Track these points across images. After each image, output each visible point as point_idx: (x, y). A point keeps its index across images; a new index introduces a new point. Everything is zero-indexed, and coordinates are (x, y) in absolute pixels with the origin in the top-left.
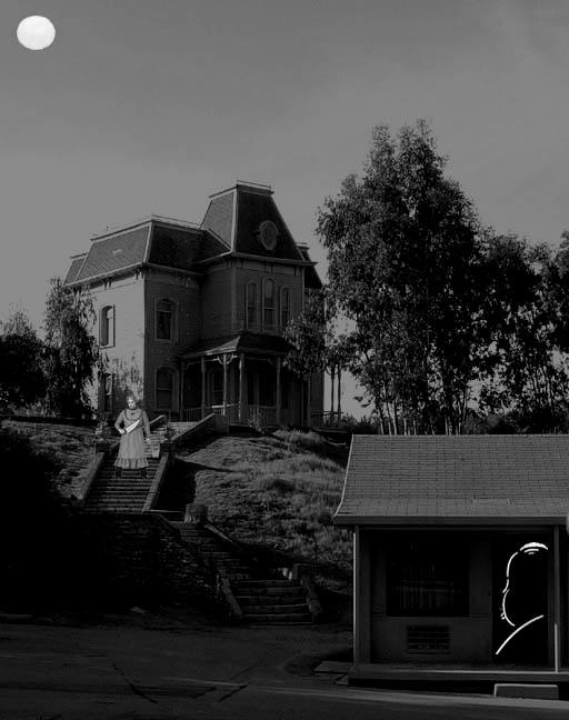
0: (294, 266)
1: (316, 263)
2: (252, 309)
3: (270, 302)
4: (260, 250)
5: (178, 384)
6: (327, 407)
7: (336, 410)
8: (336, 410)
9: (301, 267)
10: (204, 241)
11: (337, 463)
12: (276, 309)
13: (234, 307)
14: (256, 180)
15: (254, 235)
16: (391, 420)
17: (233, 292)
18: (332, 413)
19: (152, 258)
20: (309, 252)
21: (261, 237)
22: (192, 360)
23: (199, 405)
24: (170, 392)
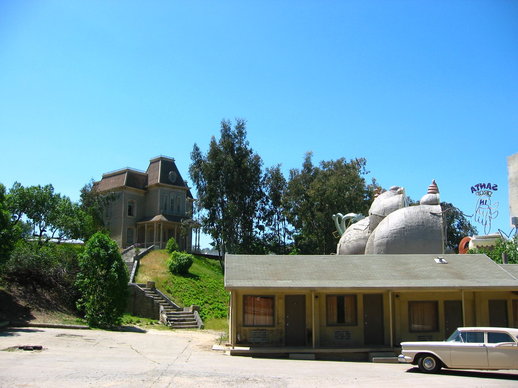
0: (183, 189)
1: (175, 160)
2: (166, 205)
3: (172, 200)
4: (169, 182)
5: (136, 233)
6: (193, 244)
7: (197, 245)
8: (197, 245)
9: (185, 190)
10: (145, 177)
11: (192, 230)
12: (175, 206)
13: (159, 204)
14: (168, 154)
15: (168, 176)
16: (255, 333)
17: (159, 199)
18: (196, 246)
19: (128, 184)
20: (187, 184)
21: (170, 178)
22: (141, 225)
23: (144, 243)
24: (132, 237)
